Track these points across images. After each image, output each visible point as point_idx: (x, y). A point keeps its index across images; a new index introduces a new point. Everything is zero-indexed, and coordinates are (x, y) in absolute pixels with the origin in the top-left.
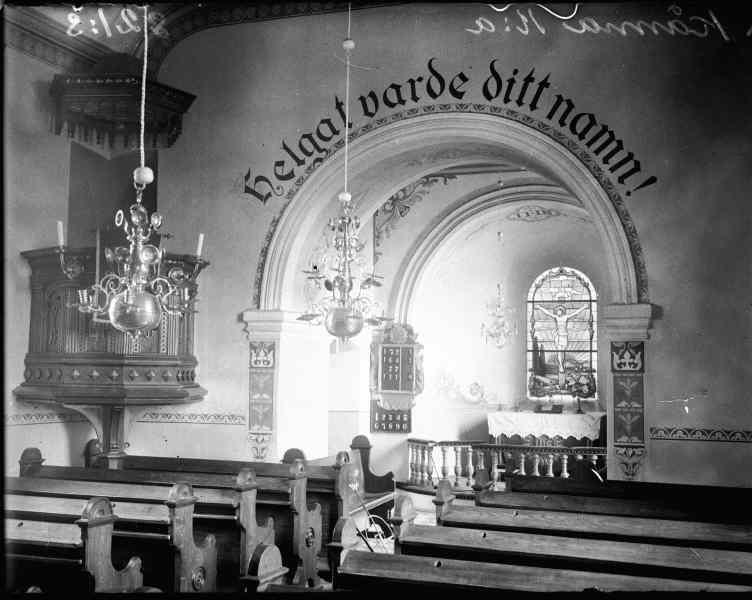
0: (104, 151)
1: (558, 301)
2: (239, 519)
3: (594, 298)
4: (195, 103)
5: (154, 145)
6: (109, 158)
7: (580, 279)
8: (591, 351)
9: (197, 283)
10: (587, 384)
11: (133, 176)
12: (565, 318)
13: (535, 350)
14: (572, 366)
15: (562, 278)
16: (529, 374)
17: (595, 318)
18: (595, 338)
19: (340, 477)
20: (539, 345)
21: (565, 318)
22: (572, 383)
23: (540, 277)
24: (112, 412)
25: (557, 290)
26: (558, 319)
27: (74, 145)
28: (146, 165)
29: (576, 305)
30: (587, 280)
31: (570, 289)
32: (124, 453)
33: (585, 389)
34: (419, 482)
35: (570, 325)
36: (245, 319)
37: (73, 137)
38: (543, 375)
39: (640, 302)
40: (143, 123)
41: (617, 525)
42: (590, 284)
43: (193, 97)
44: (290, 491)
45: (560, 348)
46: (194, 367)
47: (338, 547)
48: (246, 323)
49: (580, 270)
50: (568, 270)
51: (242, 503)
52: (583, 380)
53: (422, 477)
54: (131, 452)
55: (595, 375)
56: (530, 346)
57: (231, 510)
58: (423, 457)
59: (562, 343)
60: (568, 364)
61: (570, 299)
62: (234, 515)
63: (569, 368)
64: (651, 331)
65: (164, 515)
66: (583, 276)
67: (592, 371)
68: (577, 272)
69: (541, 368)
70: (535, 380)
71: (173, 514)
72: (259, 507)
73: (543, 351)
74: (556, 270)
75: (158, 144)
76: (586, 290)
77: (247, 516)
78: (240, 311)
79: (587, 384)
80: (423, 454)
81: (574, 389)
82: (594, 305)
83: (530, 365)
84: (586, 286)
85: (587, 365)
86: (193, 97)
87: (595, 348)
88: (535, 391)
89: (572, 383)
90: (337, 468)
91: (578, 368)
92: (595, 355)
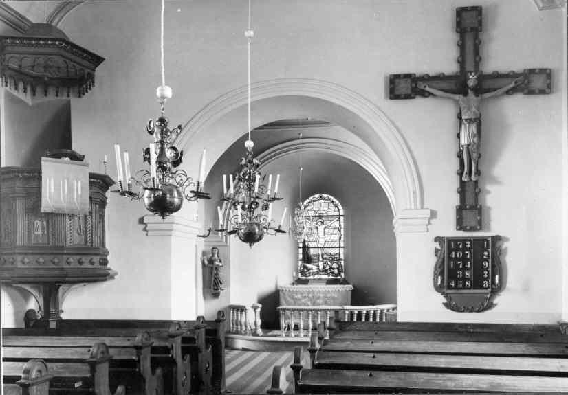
0: (27, 99)
1: (319, 216)
2: (172, 356)
3: (342, 213)
4: (104, 62)
5: (68, 96)
6: (30, 104)
7: (333, 202)
8: (340, 247)
9: (107, 196)
10: (338, 269)
11: (156, 92)
12: (323, 226)
13: (304, 247)
14: (328, 257)
15: (321, 201)
16: (300, 263)
17: (342, 226)
18: (342, 239)
19: (221, 327)
20: (306, 244)
21: (323, 226)
22: (328, 267)
23: (307, 201)
24: (51, 291)
25: (317, 209)
26: (319, 227)
27: (7, 92)
28: (166, 85)
29: (330, 219)
30: (337, 202)
31: (326, 209)
32: (60, 317)
33: (336, 271)
34: (243, 332)
35: (327, 231)
36: (145, 222)
37: (6, 86)
38: (308, 263)
39: (422, 208)
40: (162, 50)
41: (483, 348)
42: (339, 204)
43: (103, 59)
44: (195, 337)
45: (320, 246)
46: (106, 256)
47: (298, 367)
48: (146, 225)
49: (332, 196)
50: (325, 196)
51: (174, 346)
52: (335, 266)
53: (237, 328)
54: (64, 316)
55: (342, 262)
56: (301, 245)
57: (167, 350)
58: (237, 316)
59: (321, 243)
60: (325, 256)
61: (326, 215)
62: (169, 353)
63: (326, 258)
64: (429, 227)
65: (133, 355)
66: (335, 200)
67: (340, 259)
68: (330, 197)
69: (307, 259)
70: (304, 267)
71: (138, 355)
72: (183, 349)
73: (308, 248)
74: (317, 196)
75: (71, 95)
76: (336, 209)
77: (177, 353)
78: (141, 216)
79: (338, 269)
80: (237, 313)
81: (329, 272)
82: (342, 218)
83: (301, 257)
84: (337, 206)
85: (337, 256)
86: (103, 59)
87: (342, 245)
88: (303, 274)
89: (328, 267)
90: (218, 321)
91: (333, 259)
92: (342, 250)
